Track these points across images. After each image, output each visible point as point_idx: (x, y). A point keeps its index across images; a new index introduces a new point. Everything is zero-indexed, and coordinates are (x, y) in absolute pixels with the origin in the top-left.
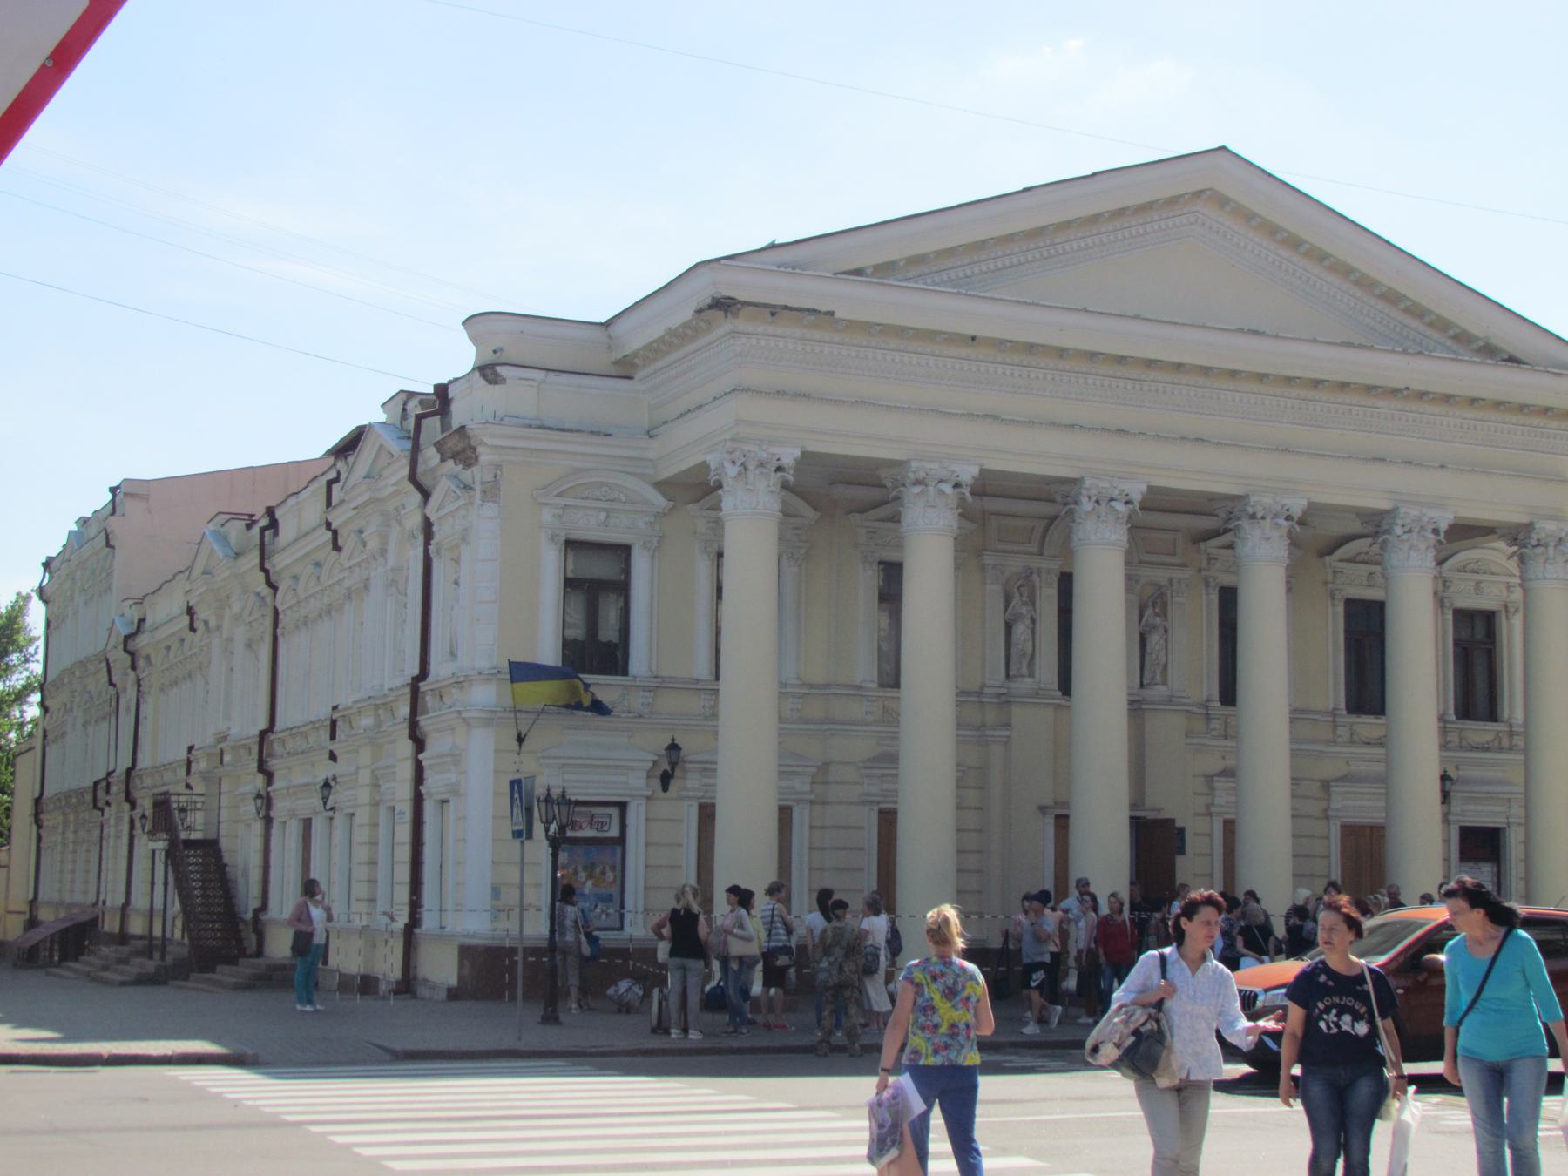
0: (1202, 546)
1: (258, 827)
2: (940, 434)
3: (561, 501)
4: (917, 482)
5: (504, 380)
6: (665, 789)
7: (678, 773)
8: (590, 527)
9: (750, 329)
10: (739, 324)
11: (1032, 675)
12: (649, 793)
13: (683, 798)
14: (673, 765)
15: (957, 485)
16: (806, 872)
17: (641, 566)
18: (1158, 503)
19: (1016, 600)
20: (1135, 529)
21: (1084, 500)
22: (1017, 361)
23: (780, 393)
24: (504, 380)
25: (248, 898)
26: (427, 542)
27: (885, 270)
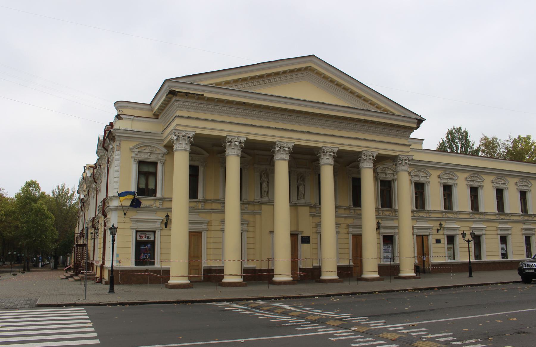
2: (238, 131)
4: (229, 142)
5: (122, 119)
8: (145, 157)
9: (180, 99)
10: (178, 98)
11: (268, 196)
14: (167, 220)
15: (240, 143)
17: (160, 167)
19: (263, 177)
24: (122, 119)
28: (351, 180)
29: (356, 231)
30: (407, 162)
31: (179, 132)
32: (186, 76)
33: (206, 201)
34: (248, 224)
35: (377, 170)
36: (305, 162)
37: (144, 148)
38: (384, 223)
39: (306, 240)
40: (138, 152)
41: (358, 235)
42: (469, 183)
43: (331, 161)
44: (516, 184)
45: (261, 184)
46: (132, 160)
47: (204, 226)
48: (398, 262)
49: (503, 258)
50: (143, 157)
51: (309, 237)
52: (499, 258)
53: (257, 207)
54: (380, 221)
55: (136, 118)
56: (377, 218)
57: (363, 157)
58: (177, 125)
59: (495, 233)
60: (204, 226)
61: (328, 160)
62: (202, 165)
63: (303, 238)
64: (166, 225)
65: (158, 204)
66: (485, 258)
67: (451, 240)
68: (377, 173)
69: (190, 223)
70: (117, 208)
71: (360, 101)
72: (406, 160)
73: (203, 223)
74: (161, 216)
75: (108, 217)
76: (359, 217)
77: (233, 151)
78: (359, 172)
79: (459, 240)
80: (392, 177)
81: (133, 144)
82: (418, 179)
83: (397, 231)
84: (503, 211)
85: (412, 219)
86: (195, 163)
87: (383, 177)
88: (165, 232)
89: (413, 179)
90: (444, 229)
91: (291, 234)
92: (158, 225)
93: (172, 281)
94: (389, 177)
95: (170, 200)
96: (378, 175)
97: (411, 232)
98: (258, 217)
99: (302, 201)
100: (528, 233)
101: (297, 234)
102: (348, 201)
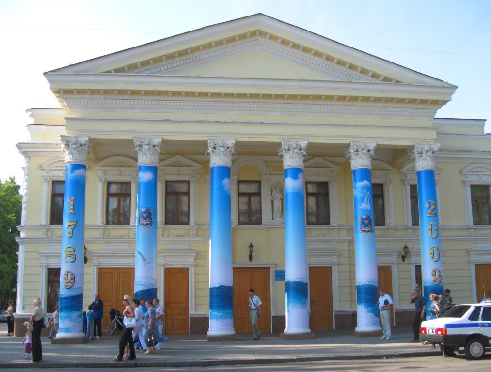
6: (403, 261)
7: (407, 256)
12: (398, 262)
13: (92, 266)
16: (194, 290)
19: (274, 192)
22: (114, 98)
27: (132, 68)
32: (71, 65)
40: (50, 169)
47: (334, 259)
60: (334, 259)
63: (276, 272)
64: (403, 258)
69: (420, 255)
73: (392, 255)
74: (399, 247)
92: (395, 259)
93: (59, 335)
96: (405, 177)
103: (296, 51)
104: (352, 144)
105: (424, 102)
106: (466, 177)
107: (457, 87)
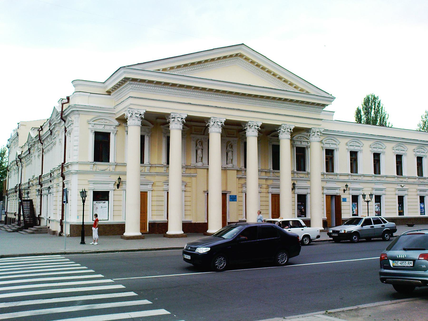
0: (240, 133)
1: (39, 196)
3: (94, 123)
4: (173, 118)
6: (118, 188)
8: (101, 129)
14: (119, 183)
15: (182, 119)
17: (112, 137)
18: (228, 123)
20: (223, 128)
21: (211, 122)
23: (228, 108)
25: (37, 213)
26: (65, 133)
28: (271, 147)
29: (275, 191)
30: (319, 134)
31: (133, 110)
33: (151, 166)
34: (185, 185)
35: (294, 138)
36: (234, 132)
37: (99, 121)
38: (298, 184)
39: (233, 198)
40: (95, 124)
41: (277, 194)
42: (373, 150)
43: (256, 133)
44: (414, 150)
45: (197, 151)
46: (90, 131)
48: (309, 218)
49: (399, 215)
50: (98, 128)
51: (236, 196)
52: (418, 215)
53: (192, 171)
54: (295, 183)
55: (92, 95)
56: (292, 180)
57: (282, 129)
58: (131, 104)
59: (394, 193)
61: (253, 133)
62: (147, 135)
64: (118, 186)
65: (112, 168)
66: (406, 215)
67: (355, 199)
68: (294, 141)
70: (77, 173)
71: (282, 82)
72: (318, 132)
74: (115, 178)
75: (66, 179)
76: (278, 179)
77: (176, 125)
78: (278, 141)
79: (361, 199)
80: (307, 144)
81: (90, 117)
82: (329, 146)
83: (308, 191)
84: (402, 174)
85: (322, 181)
86: (143, 134)
87: (298, 144)
88: (118, 192)
89: (324, 146)
90: (349, 190)
91: (222, 193)
94: (304, 145)
95: (124, 165)
96: (294, 142)
97: (321, 192)
98: (194, 179)
99: (230, 165)
100: (422, 194)
101: (226, 194)
102: (270, 166)
103: (257, 68)
104: (212, 118)
105: (318, 104)
106: (308, 143)
107: (334, 98)
